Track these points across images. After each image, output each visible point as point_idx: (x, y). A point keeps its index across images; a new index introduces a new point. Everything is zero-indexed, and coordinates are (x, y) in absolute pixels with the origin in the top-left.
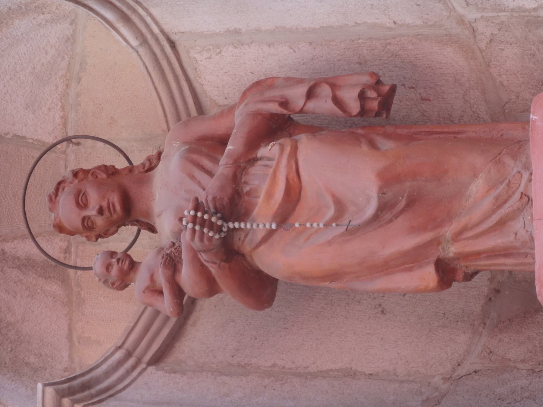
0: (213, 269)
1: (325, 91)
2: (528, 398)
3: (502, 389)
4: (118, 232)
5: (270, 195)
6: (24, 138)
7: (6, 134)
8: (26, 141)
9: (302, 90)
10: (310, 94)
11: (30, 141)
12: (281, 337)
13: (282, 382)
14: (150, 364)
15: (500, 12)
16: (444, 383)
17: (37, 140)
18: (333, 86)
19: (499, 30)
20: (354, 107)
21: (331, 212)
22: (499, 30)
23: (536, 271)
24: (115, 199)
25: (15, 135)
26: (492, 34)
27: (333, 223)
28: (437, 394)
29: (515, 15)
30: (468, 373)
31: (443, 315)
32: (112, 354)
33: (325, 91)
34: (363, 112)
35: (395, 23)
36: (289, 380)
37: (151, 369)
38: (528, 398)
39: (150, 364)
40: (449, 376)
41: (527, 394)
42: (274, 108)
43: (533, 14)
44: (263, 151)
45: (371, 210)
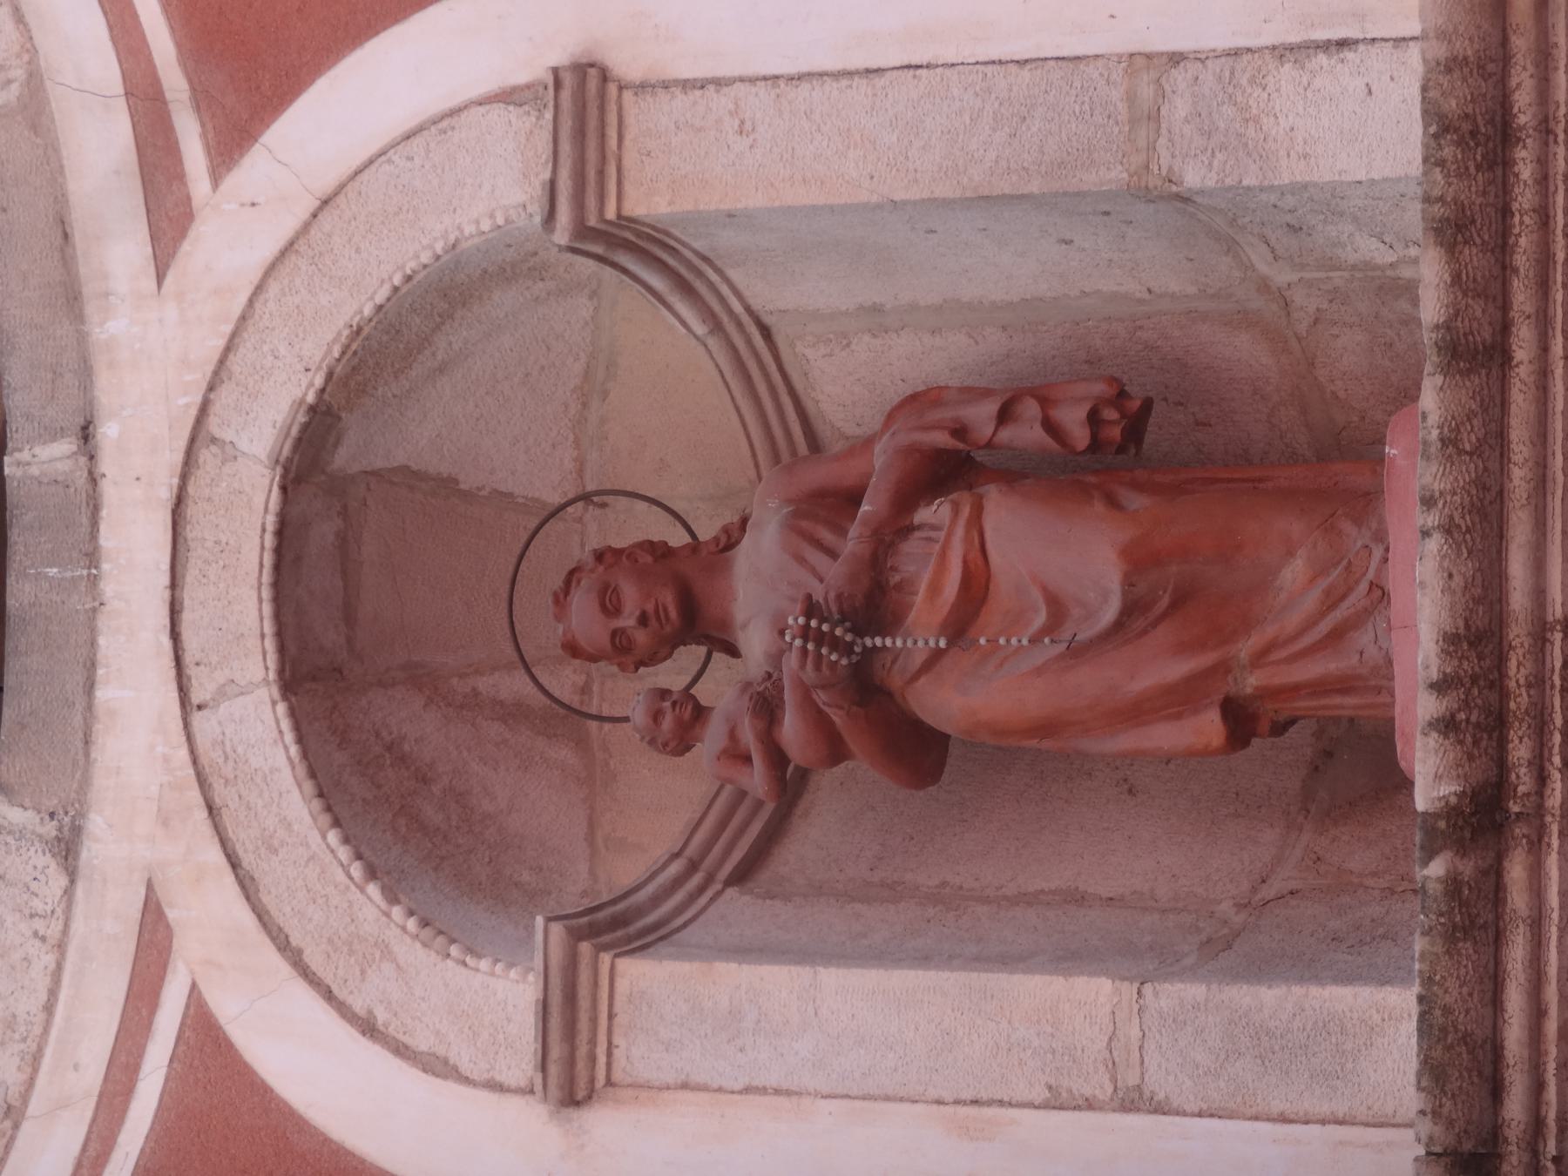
0: (837, 717)
1: (1031, 409)
2: (1384, 937)
4: (1170, 995)
5: (935, 589)
9: (990, 408)
10: (1005, 415)
13: (958, 913)
16: (1236, 914)
18: (1045, 402)
19: (1331, 301)
20: (1080, 436)
21: (1040, 619)
24: (668, 598)
26: (1318, 309)
28: (1226, 931)
29: (1358, 275)
31: (1234, 796)
33: (1031, 409)
34: (1096, 445)
35: (1149, 291)
37: (731, 892)
39: (729, 883)
40: (1247, 901)
42: (942, 439)
43: (1389, 273)
44: (923, 515)
45: (1109, 613)
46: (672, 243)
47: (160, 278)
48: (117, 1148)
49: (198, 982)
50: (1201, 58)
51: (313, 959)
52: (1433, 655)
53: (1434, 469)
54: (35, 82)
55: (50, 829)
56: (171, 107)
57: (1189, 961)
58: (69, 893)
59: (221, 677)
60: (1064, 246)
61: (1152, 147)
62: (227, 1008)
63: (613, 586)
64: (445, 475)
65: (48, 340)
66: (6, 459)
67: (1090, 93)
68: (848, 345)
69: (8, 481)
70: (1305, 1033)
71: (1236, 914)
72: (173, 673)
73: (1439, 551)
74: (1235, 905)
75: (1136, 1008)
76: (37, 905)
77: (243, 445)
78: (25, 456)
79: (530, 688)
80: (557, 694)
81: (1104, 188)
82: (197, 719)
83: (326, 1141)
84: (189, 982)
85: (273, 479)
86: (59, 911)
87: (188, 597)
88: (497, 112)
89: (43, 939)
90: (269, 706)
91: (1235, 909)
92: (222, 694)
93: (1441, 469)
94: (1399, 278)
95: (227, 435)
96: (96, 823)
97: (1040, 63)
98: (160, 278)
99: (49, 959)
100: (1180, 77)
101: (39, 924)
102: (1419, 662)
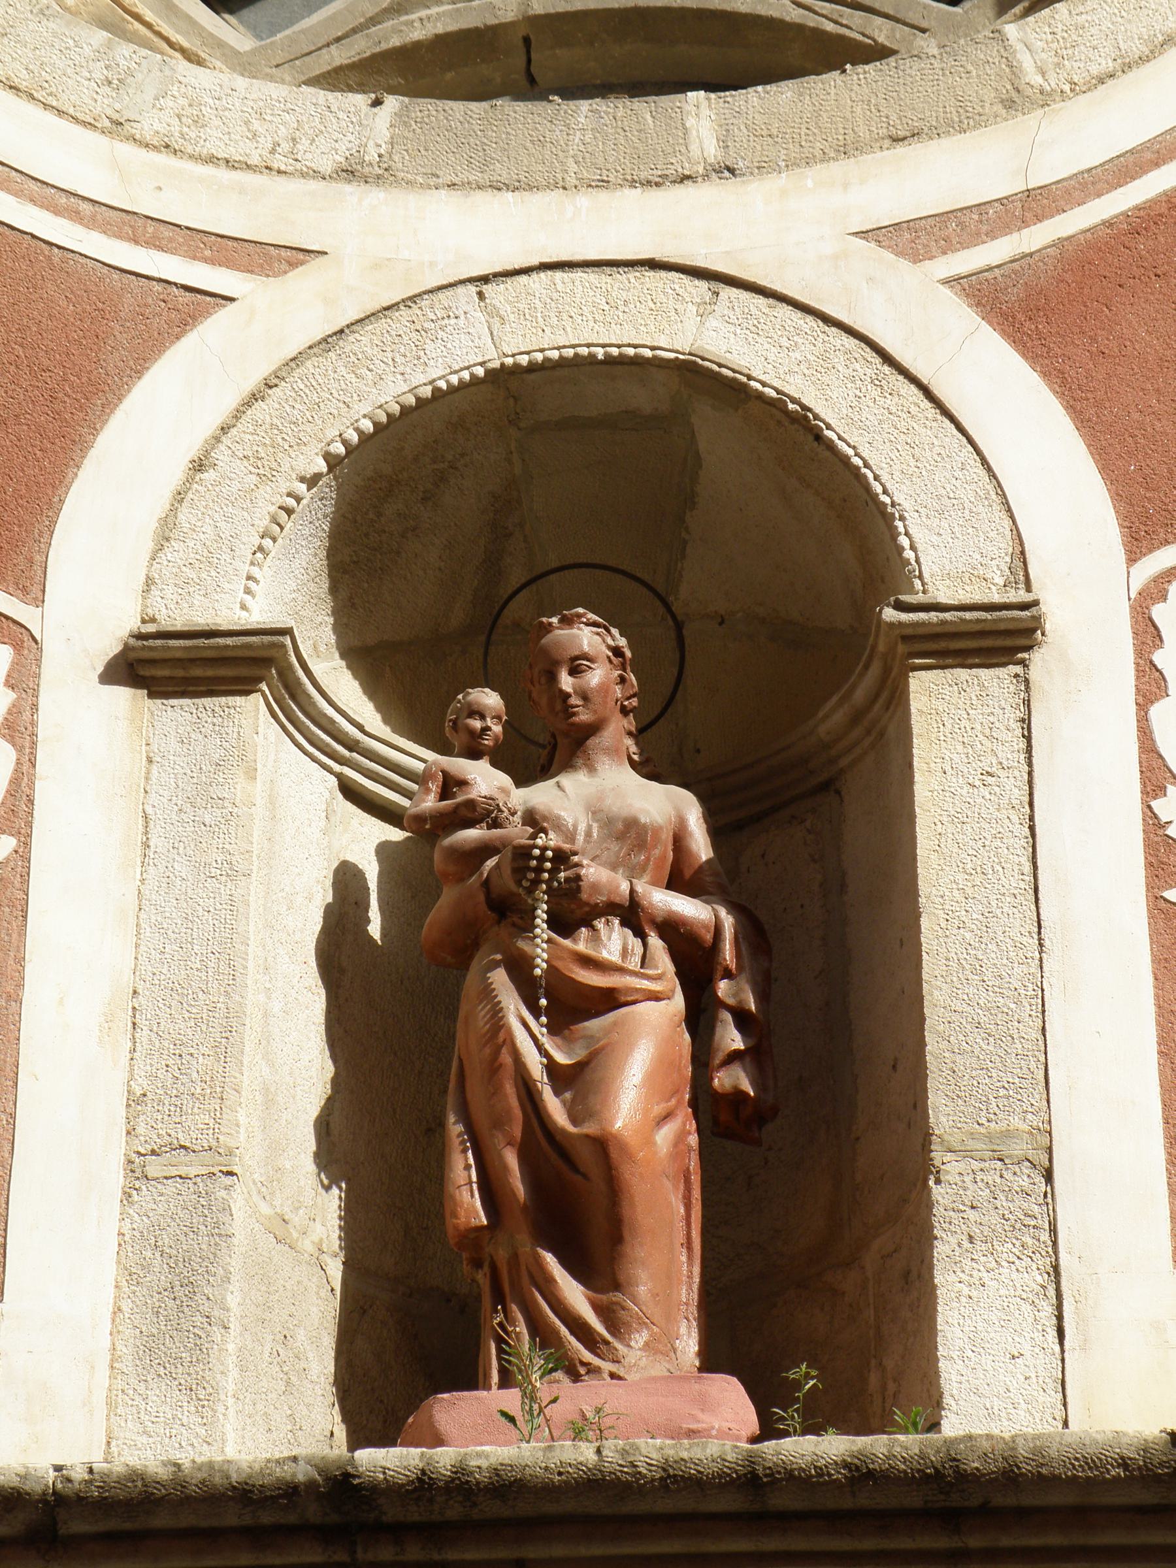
2: (288, 1383)
3: (304, 1339)
6: (684, 557)
7: (687, 529)
8: (856, 455)
11: (679, 565)
12: (389, 975)
13: (314, 987)
14: (340, 777)
15: (875, 1308)
16: (313, 1242)
17: (681, 576)
19: (850, 1305)
22: (850, 1305)
23: (475, 1393)
25: (685, 542)
26: (844, 1293)
27: (709, 861)
28: (295, 1235)
29: (872, 1333)
30: (330, 1279)
31: (425, 1226)
32: (849, 445)
35: (858, 1139)
36: (317, 998)
37: (333, 781)
38: (288, 1383)
39: (340, 777)
40: (325, 1250)
41: (294, 1379)
43: (873, 1362)
46: (892, 708)
47: (862, 234)
48: (86, 230)
49: (235, 304)
50: (1050, 1197)
51: (259, 411)
52: (493, 1460)
53: (654, 1456)
54: (1045, 98)
55: (372, 155)
56: (1016, 235)
57: (265, 1209)
58: (317, 175)
59: (506, 309)
60: (892, 1063)
61: (967, 1154)
62: (223, 317)
63: (592, 666)
64: (696, 500)
65: (786, 155)
66: (702, 92)
67: (1016, 1096)
68: (814, 861)
69: (681, 96)
70: (191, 1328)
71: (313, 1242)
72: (509, 267)
73: (581, 1463)
74: (321, 1239)
75: (215, 1170)
76: (304, 144)
77: (712, 322)
78: (705, 111)
79: (515, 581)
80: (512, 605)
81: (930, 1112)
82: (472, 289)
83: (95, 431)
84: (235, 297)
85: (683, 354)
86: (298, 166)
87: (578, 275)
88: (1003, 546)
89: (273, 151)
90: (480, 360)
91: (316, 1241)
92: (492, 312)
93: (654, 1462)
94: (869, 1371)
95: (722, 307)
96: (376, 196)
97: (1043, 1049)
98: (862, 234)
99: (255, 160)
100: (1027, 1179)
101: (285, 146)
102: (484, 1448)
